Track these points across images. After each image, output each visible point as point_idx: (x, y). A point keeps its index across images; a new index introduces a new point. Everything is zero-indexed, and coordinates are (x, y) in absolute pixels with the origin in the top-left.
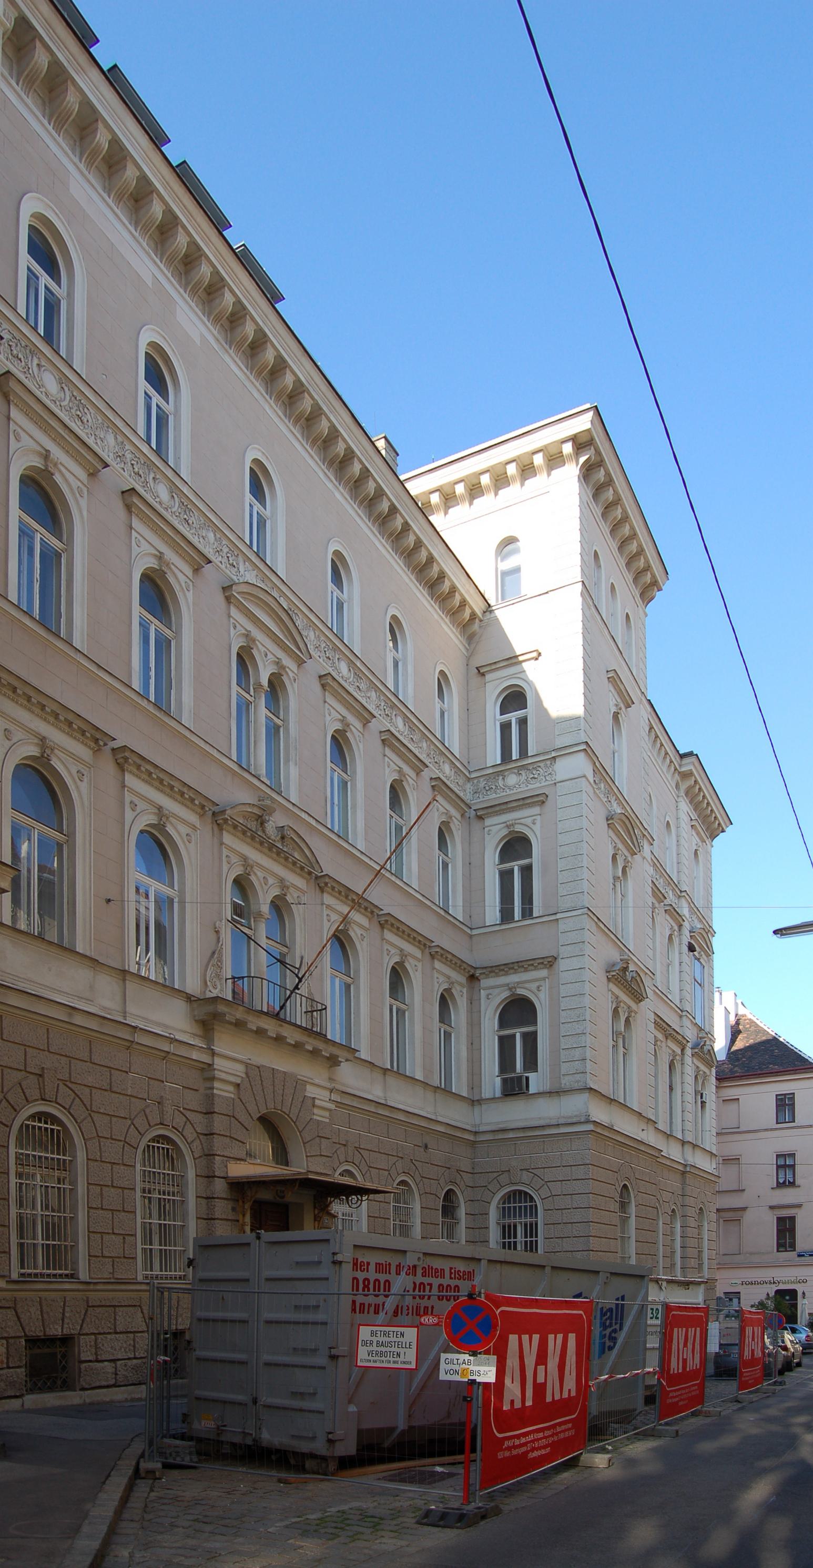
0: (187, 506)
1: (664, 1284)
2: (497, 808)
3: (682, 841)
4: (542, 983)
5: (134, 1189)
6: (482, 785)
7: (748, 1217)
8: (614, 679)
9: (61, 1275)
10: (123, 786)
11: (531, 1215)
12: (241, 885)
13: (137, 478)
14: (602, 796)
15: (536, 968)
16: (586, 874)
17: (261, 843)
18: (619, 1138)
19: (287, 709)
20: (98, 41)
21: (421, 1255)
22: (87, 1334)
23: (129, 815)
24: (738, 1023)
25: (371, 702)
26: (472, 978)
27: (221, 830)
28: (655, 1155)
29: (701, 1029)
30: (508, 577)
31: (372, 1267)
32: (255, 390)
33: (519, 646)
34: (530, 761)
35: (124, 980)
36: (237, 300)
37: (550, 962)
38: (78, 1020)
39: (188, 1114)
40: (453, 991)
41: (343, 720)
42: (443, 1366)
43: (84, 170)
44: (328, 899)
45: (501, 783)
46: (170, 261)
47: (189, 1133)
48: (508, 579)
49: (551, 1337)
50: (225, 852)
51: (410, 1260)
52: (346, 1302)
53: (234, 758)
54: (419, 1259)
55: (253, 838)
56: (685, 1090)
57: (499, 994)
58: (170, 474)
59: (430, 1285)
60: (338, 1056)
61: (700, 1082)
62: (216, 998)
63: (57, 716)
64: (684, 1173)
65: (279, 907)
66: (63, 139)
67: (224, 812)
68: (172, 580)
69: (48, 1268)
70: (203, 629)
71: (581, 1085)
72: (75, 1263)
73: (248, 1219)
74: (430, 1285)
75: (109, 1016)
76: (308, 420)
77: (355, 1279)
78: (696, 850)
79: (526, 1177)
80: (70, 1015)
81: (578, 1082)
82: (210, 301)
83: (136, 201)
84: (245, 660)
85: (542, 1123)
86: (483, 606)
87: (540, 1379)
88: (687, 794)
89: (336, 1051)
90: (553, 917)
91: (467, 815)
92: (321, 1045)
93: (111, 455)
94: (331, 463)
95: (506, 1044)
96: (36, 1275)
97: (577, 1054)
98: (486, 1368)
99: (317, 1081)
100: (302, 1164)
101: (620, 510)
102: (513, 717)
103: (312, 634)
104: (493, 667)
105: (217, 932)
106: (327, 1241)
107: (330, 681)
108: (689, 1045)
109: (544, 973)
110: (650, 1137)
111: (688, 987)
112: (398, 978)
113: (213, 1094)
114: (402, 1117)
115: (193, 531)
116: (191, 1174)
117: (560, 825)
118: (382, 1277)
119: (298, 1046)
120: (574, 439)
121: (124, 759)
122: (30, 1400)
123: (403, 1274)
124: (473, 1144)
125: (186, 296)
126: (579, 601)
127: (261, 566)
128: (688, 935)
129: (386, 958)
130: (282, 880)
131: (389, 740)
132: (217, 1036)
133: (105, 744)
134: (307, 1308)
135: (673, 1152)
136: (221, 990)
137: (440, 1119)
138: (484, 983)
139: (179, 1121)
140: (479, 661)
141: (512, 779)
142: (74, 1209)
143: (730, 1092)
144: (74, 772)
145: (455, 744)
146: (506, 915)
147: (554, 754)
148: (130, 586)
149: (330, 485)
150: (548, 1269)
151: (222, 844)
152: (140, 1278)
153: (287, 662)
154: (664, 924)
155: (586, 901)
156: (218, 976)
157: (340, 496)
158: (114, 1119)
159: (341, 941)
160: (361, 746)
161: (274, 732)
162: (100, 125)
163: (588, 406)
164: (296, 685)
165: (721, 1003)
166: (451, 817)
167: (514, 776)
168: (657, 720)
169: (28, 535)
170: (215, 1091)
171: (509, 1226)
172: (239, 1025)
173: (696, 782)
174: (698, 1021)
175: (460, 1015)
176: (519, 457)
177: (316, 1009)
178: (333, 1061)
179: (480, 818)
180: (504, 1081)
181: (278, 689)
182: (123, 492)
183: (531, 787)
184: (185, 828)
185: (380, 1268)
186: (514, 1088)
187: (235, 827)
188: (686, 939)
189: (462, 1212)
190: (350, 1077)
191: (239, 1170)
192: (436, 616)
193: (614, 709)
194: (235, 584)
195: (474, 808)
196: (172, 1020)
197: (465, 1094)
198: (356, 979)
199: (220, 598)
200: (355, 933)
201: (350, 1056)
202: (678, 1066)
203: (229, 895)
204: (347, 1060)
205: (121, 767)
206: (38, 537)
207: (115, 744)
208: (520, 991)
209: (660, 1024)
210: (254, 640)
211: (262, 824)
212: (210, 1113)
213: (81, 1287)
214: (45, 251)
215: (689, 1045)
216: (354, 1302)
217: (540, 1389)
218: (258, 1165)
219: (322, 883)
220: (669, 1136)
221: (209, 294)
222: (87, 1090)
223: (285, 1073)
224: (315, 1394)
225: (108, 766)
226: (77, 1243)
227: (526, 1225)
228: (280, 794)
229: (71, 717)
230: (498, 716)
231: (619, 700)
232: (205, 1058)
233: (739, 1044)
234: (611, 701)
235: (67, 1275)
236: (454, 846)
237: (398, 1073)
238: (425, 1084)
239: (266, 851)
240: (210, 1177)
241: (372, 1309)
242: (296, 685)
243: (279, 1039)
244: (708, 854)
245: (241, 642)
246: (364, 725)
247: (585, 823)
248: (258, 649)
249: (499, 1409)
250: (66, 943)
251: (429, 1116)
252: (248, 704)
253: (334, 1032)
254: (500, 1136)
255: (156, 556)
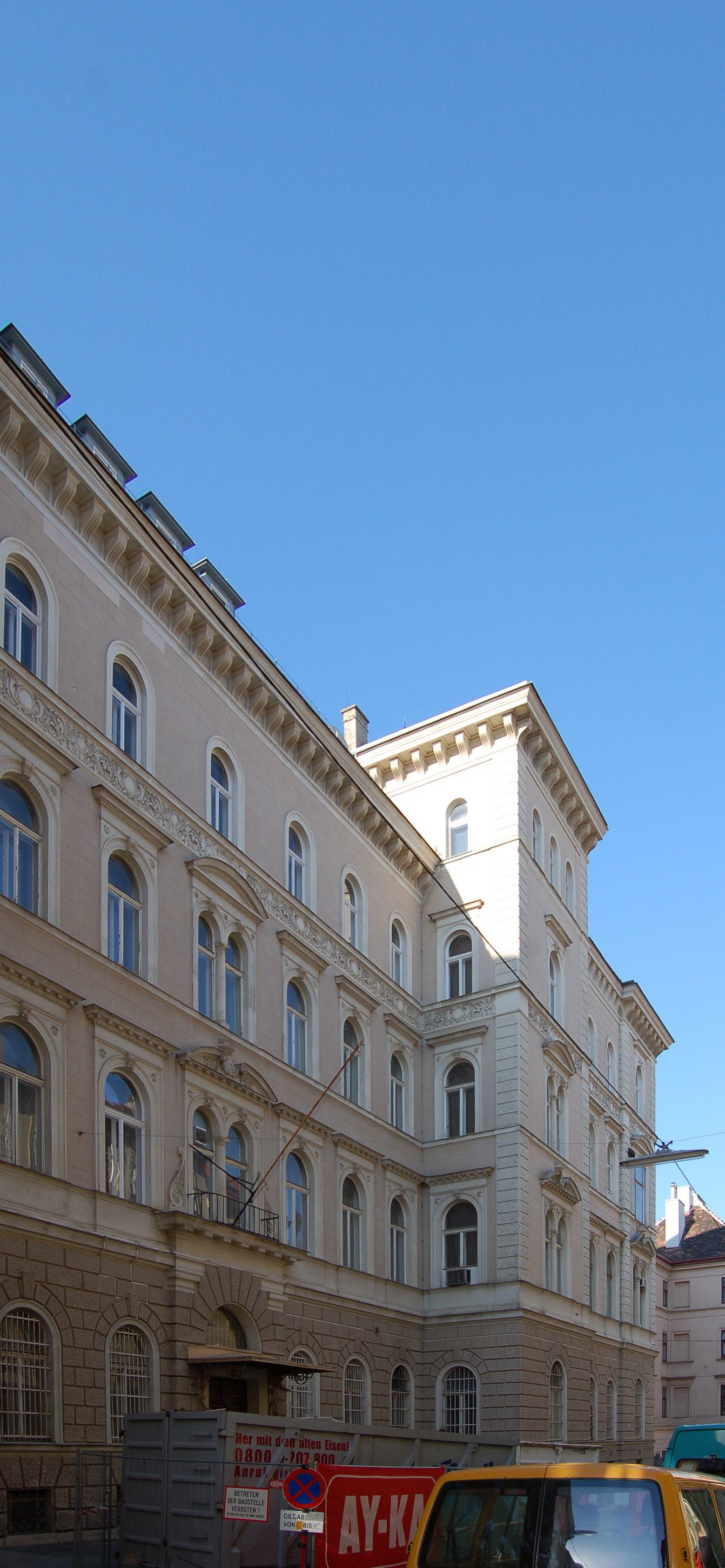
0: (152, 795)
1: (561, 1449)
2: (445, 1038)
3: (624, 1060)
4: (481, 1190)
5: (104, 1369)
6: (433, 1018)
7: (696, 1385)
8: (552, 923)
9: (39, 1439)
10: (94, 1037)
11: (471, 1388)
12: (203, 1114)
13: (106, 774)
14: (537, 1027)
15: (476, 1177)
16: (520, 1096)
17: (221, 1079)
18: (550, 1322)
19: (246, 962)
20: (69, 396)
21: (299, 1431)
22: (62, 1487)
23: (99, 1061)
24: (692, 1214)
25: (326, 952)
26: (423, 1185)
27: (184, 1069)
28: (590, 1336)
29: (641, 1224)
30: (457, 837)
31: (254, 1441)
32: (218, 688)
33: (466, 895)
34: (473, 997)
35: (95, 1198)
36: (200, 610)
37: (488, 1172)
38: (53, 1232)
39: (153, 1307)
40: (405, 1197)
41: (299, 969)
42: (282, 1520)
43: (56, 512)
44: (284, 1123)
45: (448, 1016)
46: (136, 583)
47: (154, 1323)
48: (458, 835)
49: (394, 1498)
50: (187, 1088)
51: (289, 1435)
52: (231, 1469)
53: (196, 1007)
54: (296, 1434)
55: (213, 1075)
56: (623, 1278)
57: (447, 1198)
58: (136, 768)
59: (308, 1454)
60: (289, 1257)
61: (640, 1270)
62: (175, 1213)
63: (32, 982)
64: (621, 1350)
65: (238, 1131)
66: (38, 486)
67: (185, 1055)
68: (138, 859)
69: (28, 1434)
70: (166, 898)
71: (513, 1278)
72: (52, 1429)
73: (206, 1393)
74: (308, 1454)
75: (80, 1229)
76: (267, 709)
77: (238, 1450)
78: (639, 1067)
79: (466, 1355)
80: (45, 1228)
81: (511, 1275)
82: (174, 614)
83: (105, 533)
84: (206, 923)
85: (480, 1310)
86: (435, 861)
87: (382, 1529)
88: (629, 1017)
89: (287, 1253)
90: (492, 1134)
91: (420, 1044)
92: (273, 1248)
93: (82, 757)
94: (288, 745)
95: (452, 1242)
96: (17, 1439)
97: (510, 1251)
98: (316, 1522)
99: (271, 1278)
100: (259, 1350)
101: (558, 772)
102: (460, 958)
103: (270, 897)
104: (443, 915)
105: (180, 1155)
106: (216, 1419)
107: (286, 936)
108: (628, 1238)
109: (483, 1181)
110: (585, 1320)
111: (627, 1188)
112: (351, 1188)
113: (175, 1291)
114: (353, 1306)
115: (158, 815)
116: (156, 1357)
117: (498, 1053)
118: (263, 1448)
119: (252, 1249)
120: (513, 712)
121: (93, 1014)
122: (11, 1540)
123: (282, 1445)
124: (422, 1327)
125: (152, 612)
126: (515, 856)
127: (222, 841)
128: (628, 1141)
129: (340, 1172)
130: (240, 1109)
131: (343, 983)
132: (178, 1243)
133: (76, 1004)
134: (203, 1471)
135: (612, 1332)
136: (184, 1204)
137: (390, 1307)
138: (433, 1189)
139: (145, 1313)
140: (432, 908)
141: (458, 1013)
142: (51, 1385)
143: (682, 1276)
144: (49, 1028)
145: (408, 984)
146: (453, 1130)
147: (493, 991)
148: (100, 867)
149: (288, 765)
150: (418, 1442)
151: (184, 1081)
152: (109, 1442)
153: (246, 922)
154: (604, 1134)
155: (519, 1119)
156: (181, 1192)
157: (299, 774)
158: (86, 1313)
159: (298, 1159)
160: (317, 991)
161: (233, 983)
162: (69, 473)
163: (525, 683)
164: (254, 942)
165: (676, 1196)
166: (403, 1047)
167: (460, 1010)
168: (598, 955)
169: (9, 829)
170: (177, 1288)
171: (453, 1397)
172: (198, 1233)
173: (637, 1007)
174: (639, 1218)
175: (411, 1218)
176: (466, 728)
177: (271, 1217)
178: (286, 1261)
179: (431, 1047)
180: (449, 1274)
181: (239, 945)
182: (93, 788)
183: (474, 1019)
184: (149, 1068)
185: (261, 1441)
186: (457, 1280)
187: (196, 1067)
188: (627, 1144)
189: (412, 1385)
190: (303, 1273)
191: (197, 1353)
192: (391, 872)
193: (551, 949)
194: (198, 858)
195: (425, 1038)
196: (138, 1230)
197: (415, 1285)
198: (311, 1190)
199: (183, 872)
200: (310, 1151)
201: (300, 1256)
202: (616, 1257)
203: (191, 1124)
204: (298, 1260)
205: (92, 1021)
206: (17, 831)
207: (86, 1003)
208: (463, 1197)
209: (596, 1221)
210: (214, 906)
211: (221, 1062)
212: (172, 1306)
213: (55, 1449)
214: (21, 584)
215: (628, 1238)
216: (237, 1468)
217: (381, 1540)
218: (217, 1348)
219: (278, 1110)
220: (606, 1318)
221: (173, 607)
222: (62, 1290)
223: (241, 1272)
224: (206, 1539)
225: (80, 1022)
226: (53, 1413)
227: (466, 1396)
228: (239, 1036)
229: (44, 983)
230: (448, 958)
231: (557, 940)
232: (169, 1261)
233: (692, 1233)
234: (549, 942)
235: (44, 1440)
236: (407, 1072)
237: (352, 1269)
238: (376, 1278)
239: (226, 1085)
240: (173, 1359)
241: (254, 1473)
242: (254, 942)
243: (235, 1244)
244: (652, 1070)
245: (203, 908)
246: (320, 972)
247: (519, 1051)
248: (218, 912)
249: (333, 1554)
250: (44, 1171)
251: (380, 1305)
252: (211, 959)
253: (287, 1236)
254: (445, 1321)
255: (123, 840)
